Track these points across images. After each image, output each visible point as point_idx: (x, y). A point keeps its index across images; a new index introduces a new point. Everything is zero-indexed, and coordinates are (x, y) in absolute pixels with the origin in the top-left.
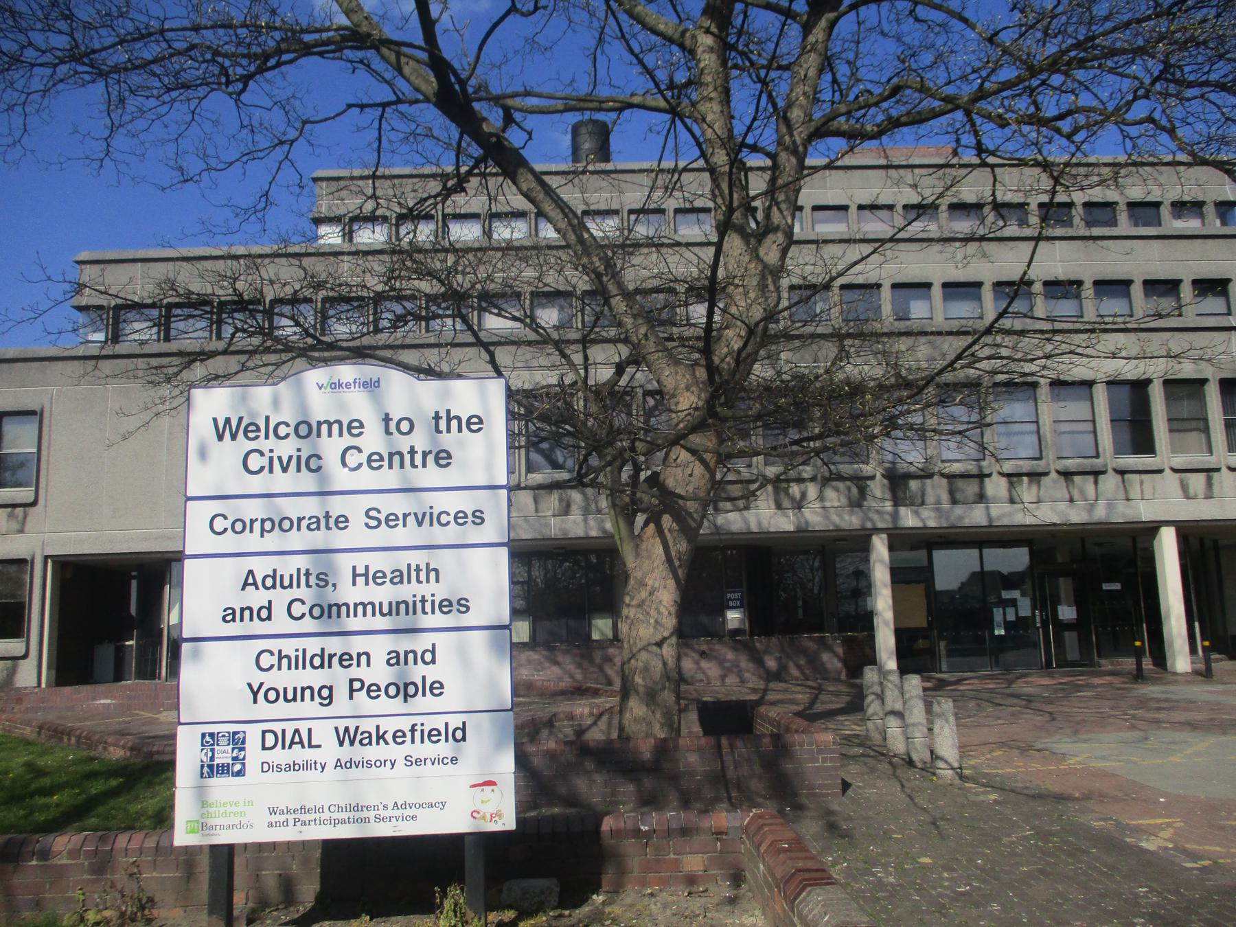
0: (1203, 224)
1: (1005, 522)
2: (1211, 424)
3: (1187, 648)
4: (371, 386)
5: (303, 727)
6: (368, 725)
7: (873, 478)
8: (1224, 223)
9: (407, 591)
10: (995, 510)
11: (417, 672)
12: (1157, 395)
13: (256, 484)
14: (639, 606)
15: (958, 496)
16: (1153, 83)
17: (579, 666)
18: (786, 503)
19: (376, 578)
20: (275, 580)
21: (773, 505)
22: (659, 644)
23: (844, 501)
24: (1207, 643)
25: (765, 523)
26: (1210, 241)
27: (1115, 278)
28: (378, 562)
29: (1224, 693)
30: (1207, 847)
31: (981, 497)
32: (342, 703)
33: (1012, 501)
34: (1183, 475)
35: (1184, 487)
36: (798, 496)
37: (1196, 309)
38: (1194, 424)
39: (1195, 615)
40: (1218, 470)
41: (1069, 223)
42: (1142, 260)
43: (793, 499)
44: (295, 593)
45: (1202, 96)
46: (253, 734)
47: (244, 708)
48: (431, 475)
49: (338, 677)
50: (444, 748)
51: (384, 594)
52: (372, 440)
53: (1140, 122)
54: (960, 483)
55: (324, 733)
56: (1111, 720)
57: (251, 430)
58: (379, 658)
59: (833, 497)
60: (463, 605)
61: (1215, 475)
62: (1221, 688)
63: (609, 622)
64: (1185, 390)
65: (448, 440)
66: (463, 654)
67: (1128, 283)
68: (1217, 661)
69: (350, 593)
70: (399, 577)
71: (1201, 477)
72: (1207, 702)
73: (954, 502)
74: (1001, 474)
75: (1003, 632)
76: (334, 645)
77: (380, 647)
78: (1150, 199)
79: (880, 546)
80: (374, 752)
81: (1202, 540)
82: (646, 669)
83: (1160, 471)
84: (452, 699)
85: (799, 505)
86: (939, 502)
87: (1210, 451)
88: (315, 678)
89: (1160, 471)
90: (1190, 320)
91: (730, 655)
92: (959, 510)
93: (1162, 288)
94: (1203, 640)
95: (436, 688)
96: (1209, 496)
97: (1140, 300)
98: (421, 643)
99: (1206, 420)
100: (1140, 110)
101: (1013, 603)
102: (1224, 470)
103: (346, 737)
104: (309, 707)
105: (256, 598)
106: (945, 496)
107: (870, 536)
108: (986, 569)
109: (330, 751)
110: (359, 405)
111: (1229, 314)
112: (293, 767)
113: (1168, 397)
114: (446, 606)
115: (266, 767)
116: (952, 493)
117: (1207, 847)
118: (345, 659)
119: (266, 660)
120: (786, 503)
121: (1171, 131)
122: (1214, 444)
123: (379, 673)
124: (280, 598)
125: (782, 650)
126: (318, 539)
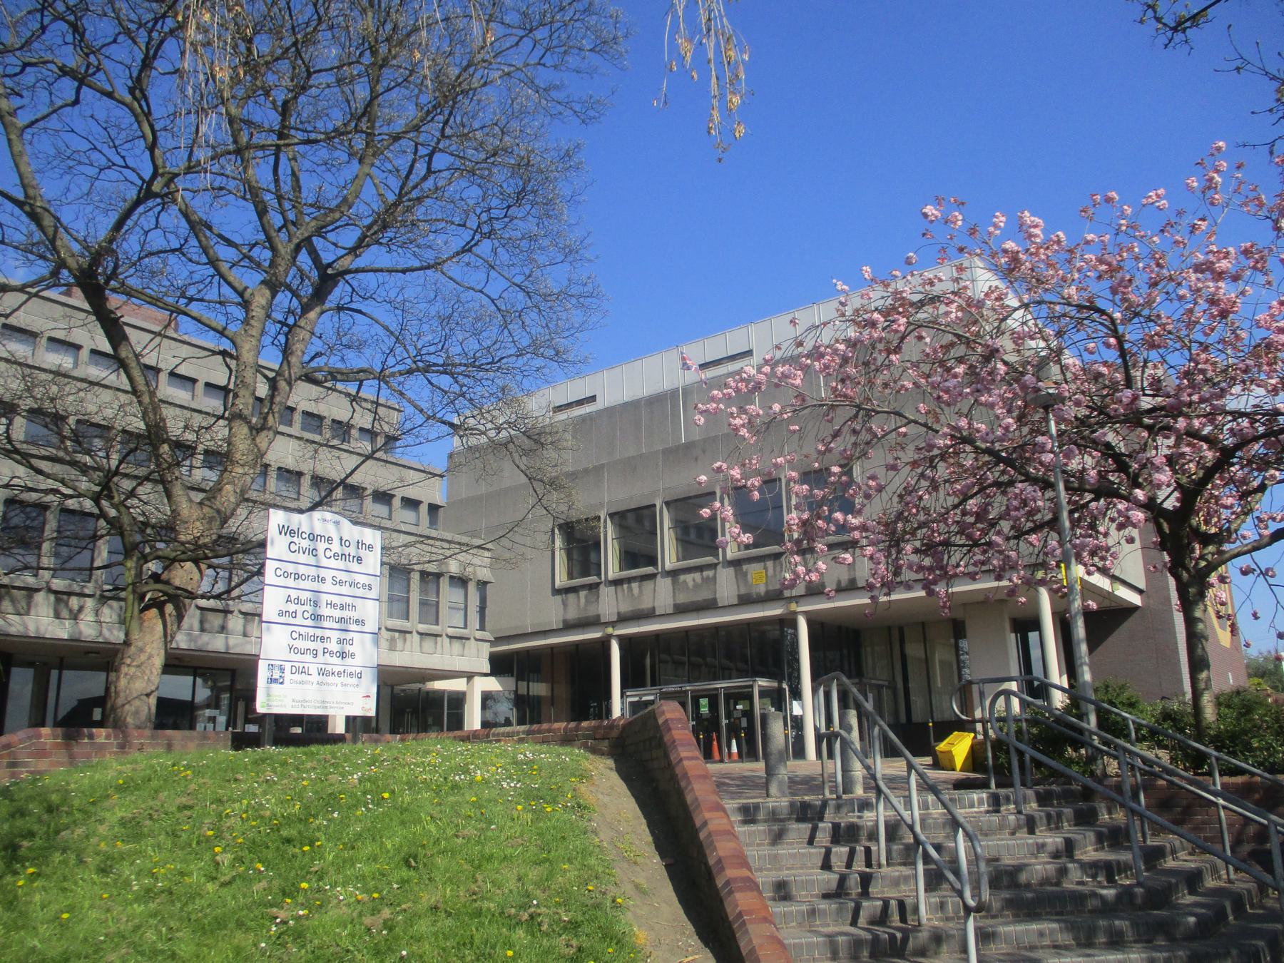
1: (237, 650)
4: (337, 523)
5: (306, 665)
6: (329, 668)
9: (346, 614)
10: (234, 640)
11: (348, 648)
13: (292, 557)
14: (138, 666)
15: (207, 626)
18: (65, 613)
19: (334, 606)
20: (298, 601)
21: (52, 614)
22: (148, 695)
23: (115, 617)
25: (42, 630)
28: (336, 600)
31: (223, 629)
32: (320, 658)
33: (245, 635)
36: (76, 608)
40: (411, 633)
41: (290, 424)
42: (334, 465)
43: (71, 611)
44: (305, 608)
46: (288, 666)
47: (285, 655)
48: (354, 566)
50: (354, 680)
51: (337, 614)
52: (336, 547)
54: (210, 616)
55: (313, 669)
57: (292, 533)
58: (334, 640)
60: (363, 623)
65: (363, 553)
66: (363, 643)
69: (326, 611)
70: (342, 607)
73: (202, 630)
74: (241, 612)
76: (319, 632)
77: (335, 635)
80: (331, 679)
82: (137, 713)
84: (358, 660)
85: (75, 616)
86: (191, 629)
87: (408, 619)
88: (312, 645)
92: (205, 637)
95: (353, 655)
98: (349, 636)
103: (322, 672)
104: (308, 657)
105: (292, 607)
106: (196, 625)
109: (315, 678)
110: (332, 531)
112: (302, 682)
114: (357, 621)
115: (292, 682)
116: (202, 622)
118: (322, 639)
119: (295, 635)
120: (65, 613)
123: (333, 646)
124: (300, 609)
126: (315, 586)
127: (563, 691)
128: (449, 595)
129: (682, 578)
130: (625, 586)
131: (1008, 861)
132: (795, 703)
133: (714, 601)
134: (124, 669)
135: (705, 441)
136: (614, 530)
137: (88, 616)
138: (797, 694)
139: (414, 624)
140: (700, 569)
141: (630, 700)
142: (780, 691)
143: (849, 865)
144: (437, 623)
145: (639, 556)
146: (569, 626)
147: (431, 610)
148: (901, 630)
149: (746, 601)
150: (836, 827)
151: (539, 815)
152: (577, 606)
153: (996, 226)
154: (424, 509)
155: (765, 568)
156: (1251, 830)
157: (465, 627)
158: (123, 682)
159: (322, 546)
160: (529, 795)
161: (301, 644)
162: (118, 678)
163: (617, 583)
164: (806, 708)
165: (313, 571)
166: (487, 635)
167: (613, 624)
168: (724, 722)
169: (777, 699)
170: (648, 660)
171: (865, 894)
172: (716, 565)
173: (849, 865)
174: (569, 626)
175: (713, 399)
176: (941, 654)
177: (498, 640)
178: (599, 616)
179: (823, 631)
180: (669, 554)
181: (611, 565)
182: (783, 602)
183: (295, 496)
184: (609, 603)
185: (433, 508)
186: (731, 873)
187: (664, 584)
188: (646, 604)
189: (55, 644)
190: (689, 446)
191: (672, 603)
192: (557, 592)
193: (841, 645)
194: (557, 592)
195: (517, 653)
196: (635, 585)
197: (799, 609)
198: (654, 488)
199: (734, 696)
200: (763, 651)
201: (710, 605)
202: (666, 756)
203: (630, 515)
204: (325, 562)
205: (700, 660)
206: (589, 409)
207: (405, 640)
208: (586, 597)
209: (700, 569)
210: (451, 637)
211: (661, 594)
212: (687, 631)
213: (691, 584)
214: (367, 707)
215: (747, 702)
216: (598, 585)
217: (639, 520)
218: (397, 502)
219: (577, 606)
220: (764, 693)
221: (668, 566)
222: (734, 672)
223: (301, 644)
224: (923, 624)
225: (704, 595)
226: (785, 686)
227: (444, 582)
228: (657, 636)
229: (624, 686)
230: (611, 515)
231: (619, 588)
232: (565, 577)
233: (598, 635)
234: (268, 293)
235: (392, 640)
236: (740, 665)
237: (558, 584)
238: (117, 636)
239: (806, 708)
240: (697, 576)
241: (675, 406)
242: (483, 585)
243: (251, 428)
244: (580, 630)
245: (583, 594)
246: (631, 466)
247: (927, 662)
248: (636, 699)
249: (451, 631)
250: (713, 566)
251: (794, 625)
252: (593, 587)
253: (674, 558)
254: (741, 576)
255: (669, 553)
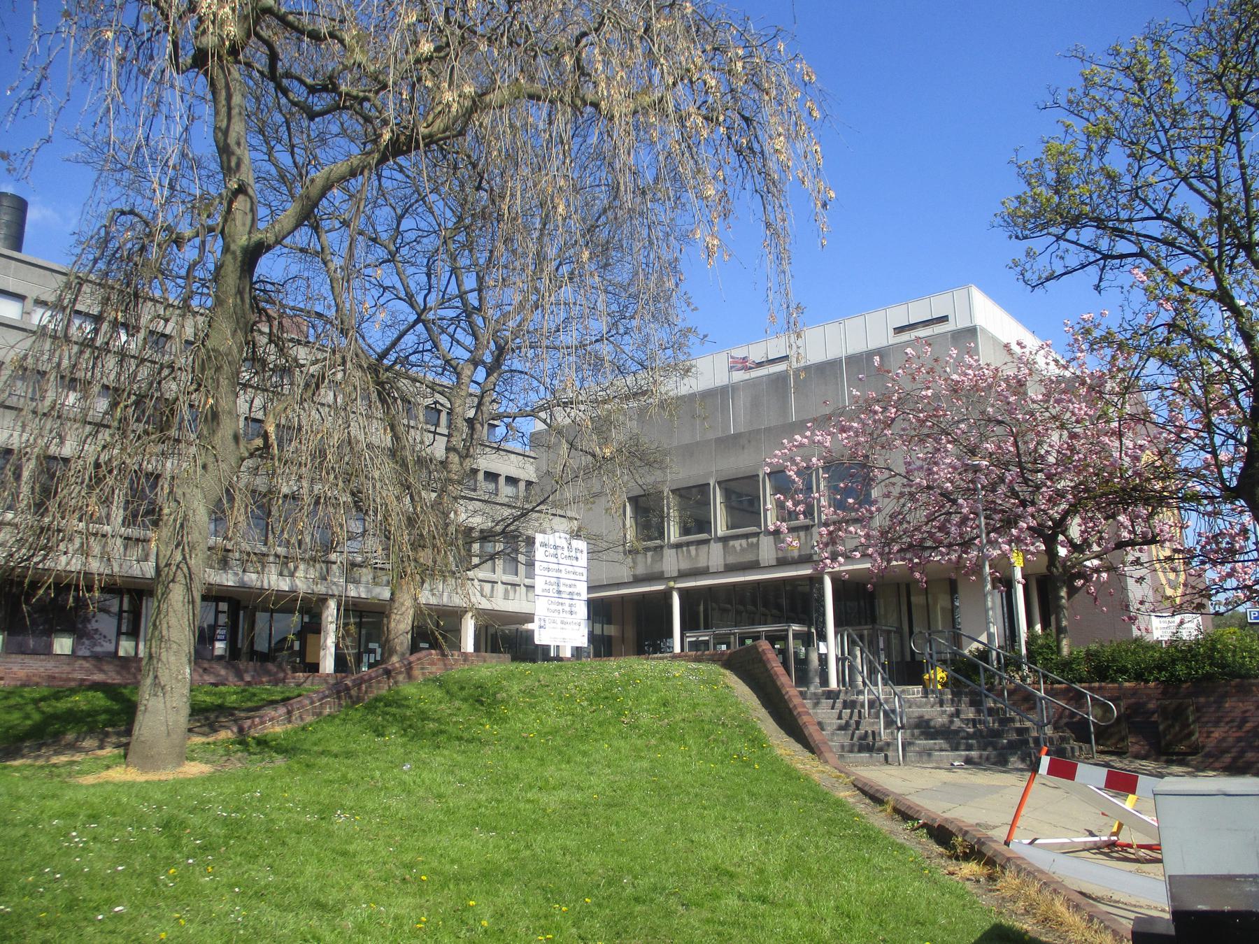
7: (335, 563)
17: (118, 673)
48: (574, 563)
49: (560, 608)
56: (324, 760)
59: (312, 574)
63: (133, 644)
65: (579, 555)
69: (562, 588)
71: (489, 585)
79: (332, 604)
85: (292, 575)
91: (223, 672)
92: (377, 590)
101: (374, 651)
104: (556, 614)
105: (547, 587)
107: (326, 600)
120: (285, 572)
125: (255, 670)
127: (630, 633)
129: (731, 543)
131: (926, 717)
132: (821, 644)
134: (393, 616)
135: (750, 432)
137: (300, 573)
138: (823, 637)
140: (746, 536)
142: (809, 634)
143: (851, 718)
146: (637, 580)
149: (782, 562)
150: (845, 702)
151: (712, 690)
153: (951, 356)
154: (522, 485)
156: (1067, 712)
158: (393, 625)
159: (559, 552)
160: (704, 682)
161: (553, 607)
162: (389, 622)
163: (678, 546)
164: (830, 647)
165: (556, 566)
167: (674, 579)
169: (807, 640)
171: (857, 728)
173: (851, 718)
175: (775, 456)
176: (943, 602)
179: (848, 590)
180: (720, 525)
184: (671, 562)
185: (529, 483)
186: (800, 710)
187: (716, 548)
188: (702, 563)
189: (280, 595)
190: (737, 436)
193: (858, 601)
196: (693, 549)
198: (710, 469)
200: (795, 602)
201: (754, 566)
202: (765, 666)
204: (561, 561)
209: (746, 536)
211: (714, 556)
213: (738, 548)
214: (583, 642)
216: (662, 547)
218: (502, 480)
220: (797, 636)
221: (720, 533)
222: (769, 618)
223: (553, 607)
225: (749, 557)
226: (813, 630)
230: (673, 491)
233: (662, 587)
234: (472, 367)
235: (506, 591)
236: (774, 611)
238: (386, 594)
239: (830, 647)
240: (744, 542)
243: (460, 457)
246: (689, 451)
247: (928, 609)
250: (757, 535)
251: (821, 582)
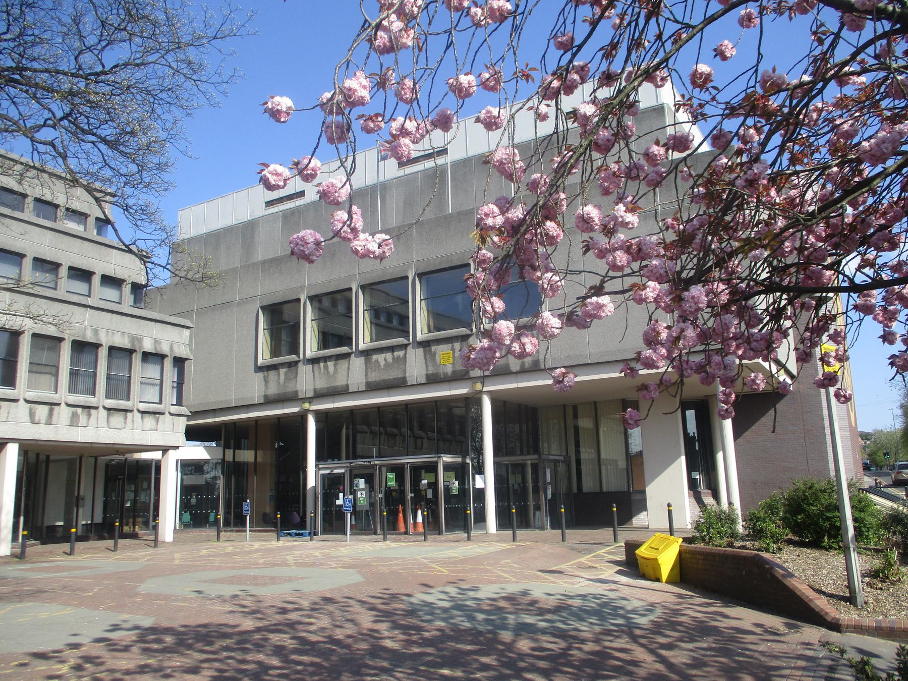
0: (85, 230)
2: (60, 371)
3: (10, 537)
8: (99, 233)
12: (25, 344)
16: (61, 119)
24: (25, 533)
26: (87, 243)
27: (13, 249)
29: (32, 570)
30: (459, 646)
34: (33, 405)
35: (32, 414)
37: (67, 286)
38: (48, 369)
39: (22, 513)
40: (59, 404)
45: (93, 143)
53: (44, 143)
61: (56, 408)
62: (29, 566)
64: (47, 343)
67: (22, 256)
68: (32, 545)
72: (16, 578)
75: (339, 502)
78: (55, 202)
81: (38, 455)
83: (16, 401)
87: (94, 394)
89: (16, 401)
90: (60, 294)
93: (50, 266)
94: (24, 530)
96: (49, 423)
97: (28, 272)
99: (58, 368)
100: (47, 134)
102: (63, 405)
108: (253, 452)
111: (89, 296)
113: (34, 346)
117: (459, 646)
121: (64, 157)
122: (59, 385)
128: (140, 371)
129: (375, 357)
130: (322, 364)
132: (477, 476)
133: (404, 379)
135: (399, 228)
136: (313, 311)
138: (480, 470)
139: (100, 398)
140: (391, 349)
141: (322, 472)
144: (128, 399)
145: (335, 337)
146: (269, 402)
147: (119, 387)
148: (575, 408)
149: (433, 380)
152: (276, 383)
155: (453, 349)
157: (160, 402)
163: (314, 361)
166: (183, 410)
167: (310, 400)
168: (410, 495)
170: (340, 433)
172: (406, 345)
174: (269, 402)
177: (195, 414)
178: (296, 392)
179: (506, 410)
181: (310, 344)
182: (469, 383)
183: (52, 285)
184: (307, 380)
187: (357, 363)
188: (340, 381)
191: (364, 381)
192: (259, 369)
194: (259, 369)
195: (226, 424)
196: (330, 364)
197: (485, 389)
199: (417, 470)
201: (400, 384)
203: (324, 298)
205: (395, 430)
206: (298, 202)
207: (89, 415)
208: (286, 374)
209: (391, 349)
210: (143, 412)
211: (355, 373)
212: (379, 408)
213: (382, 363)
215: (433, 475)
216: (297, 363)
217: (334, 303)
219: (276, 383)
220: (448, 467)
221: (362, 346)
222: (426, 443)
224: (595, 403)
225: (394, 374)
226: (468, 461)
227: (137, 359)
228: (352, 411)
229: (319, 458)
231: (316, 366)
232: (267, 355)
235: (74, 416)
237: (260, 361)
240: (389, 356)
241: (374, 200)
242: (179, 362)
244: (280, 405)
245: (283, 371)
248: (328, 472)
249: (143, 407)
251: (479, 403)
252: (292, 365)
253: (368, 339)
254: (430, 357)
255: (363, 334)
